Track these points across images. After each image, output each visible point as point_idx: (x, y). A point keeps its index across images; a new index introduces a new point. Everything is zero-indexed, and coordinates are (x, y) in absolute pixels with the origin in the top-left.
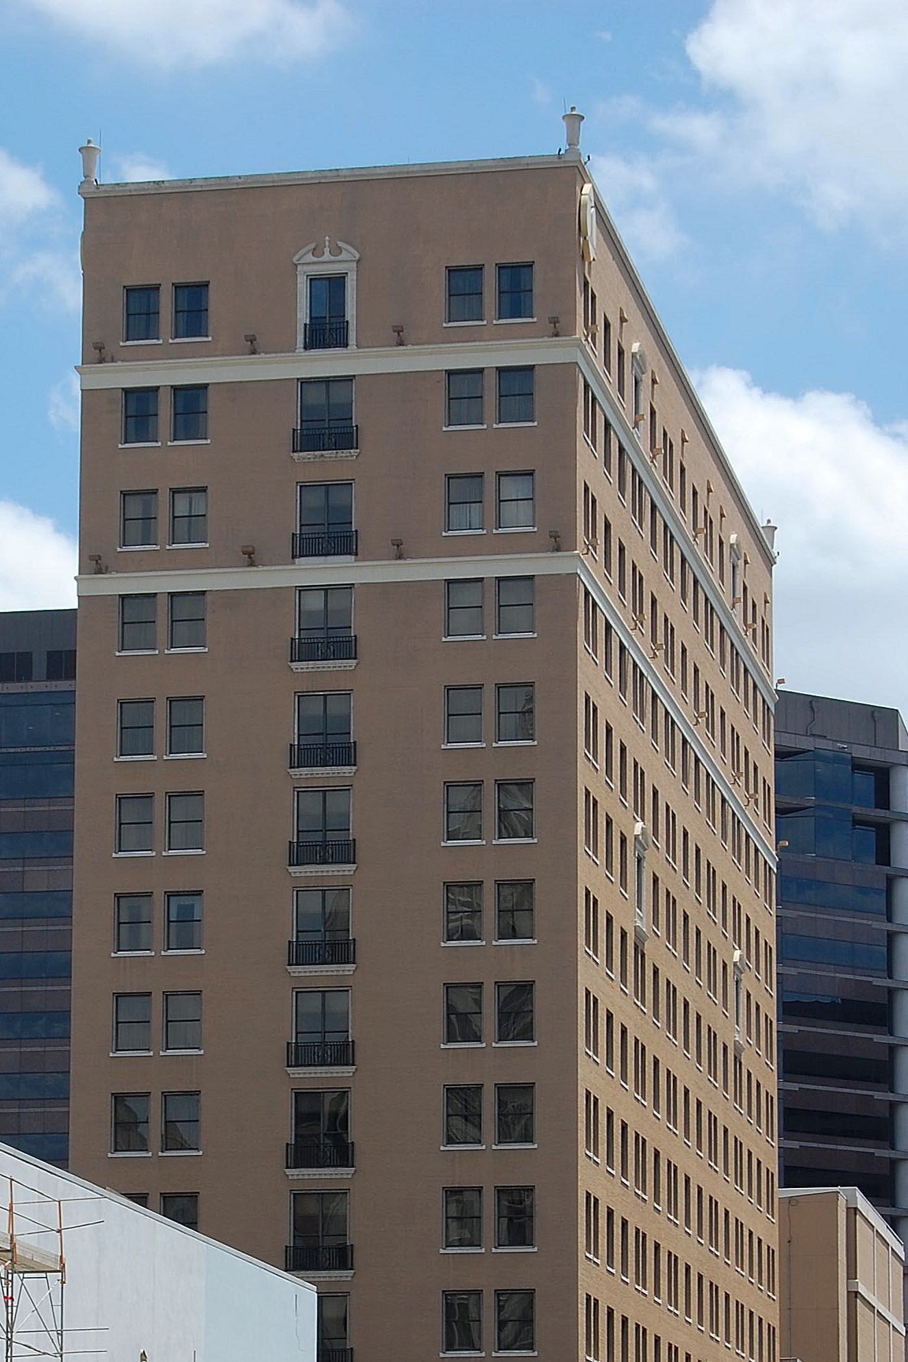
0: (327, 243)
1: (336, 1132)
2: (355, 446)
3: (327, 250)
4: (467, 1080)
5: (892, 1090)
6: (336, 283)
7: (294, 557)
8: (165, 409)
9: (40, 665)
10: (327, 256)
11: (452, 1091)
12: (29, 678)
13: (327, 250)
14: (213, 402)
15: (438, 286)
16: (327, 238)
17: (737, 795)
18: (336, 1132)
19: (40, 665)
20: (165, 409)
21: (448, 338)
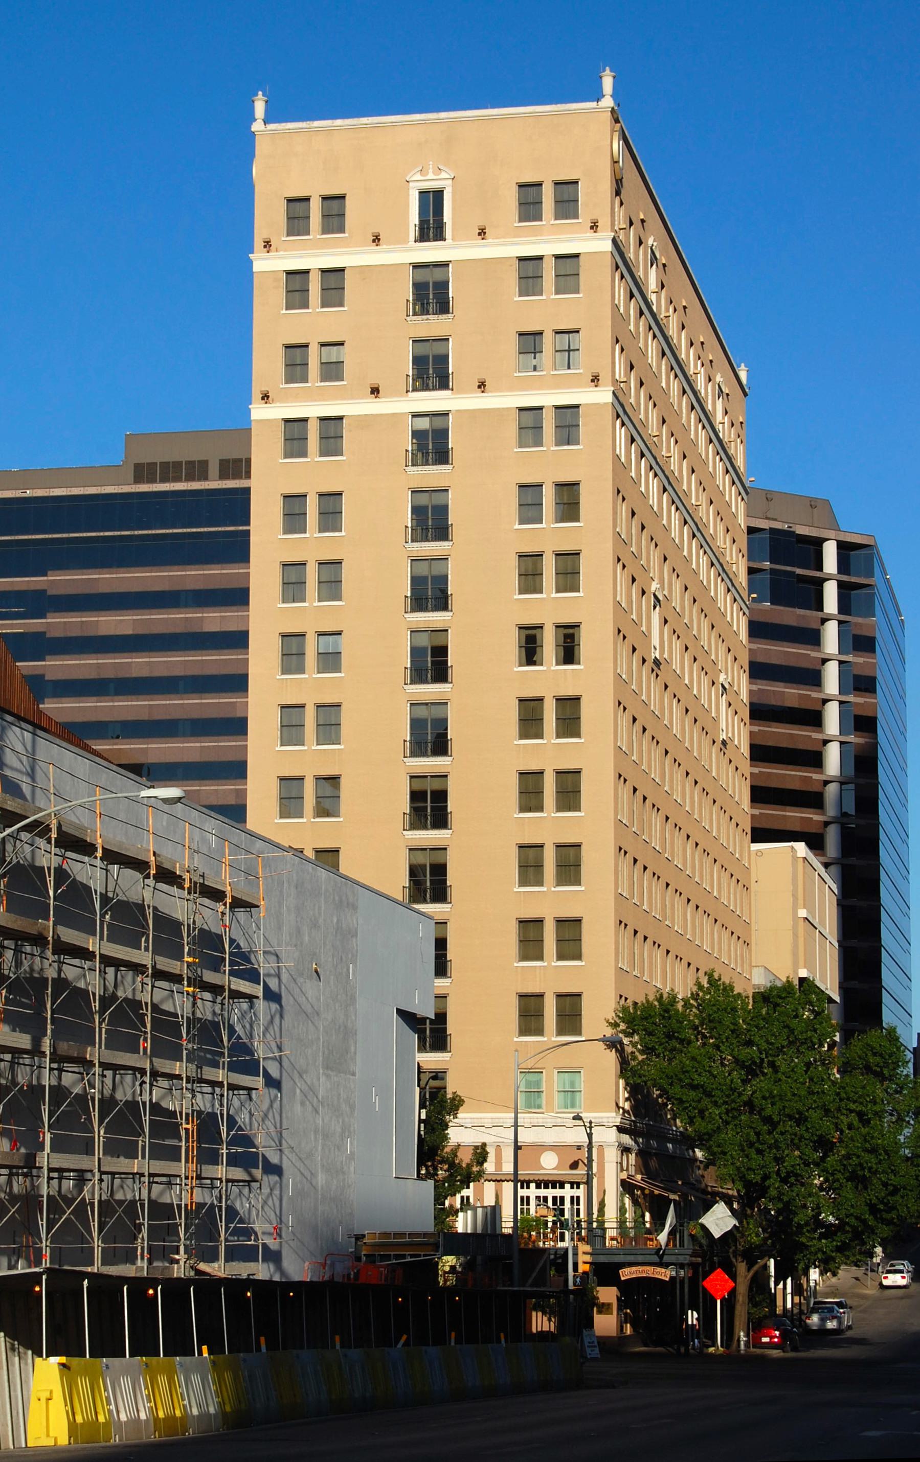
0: (431, 166)
1: (530, 1281)
2: (451, 311)
3: (431, 171)
4: (534, 767)
5: (822, 732)
6: (438, 195)
7: (407, 391)
8: (549, 271)
9: (214, 469)
10: (431, 176)
11: (523, 775)
12: (206, 479)
13: (431, 171)
14: (350, 281)
15: (511, 197)
16: (431, 163)
17: (722, 541)
18: (530, 1281)
19: (214, 469)
20: (549, 271)
21: (517, 232)
